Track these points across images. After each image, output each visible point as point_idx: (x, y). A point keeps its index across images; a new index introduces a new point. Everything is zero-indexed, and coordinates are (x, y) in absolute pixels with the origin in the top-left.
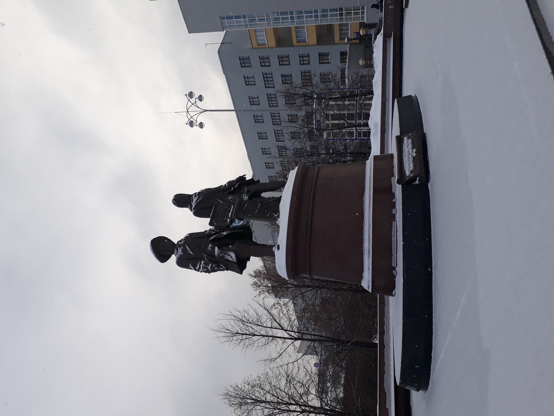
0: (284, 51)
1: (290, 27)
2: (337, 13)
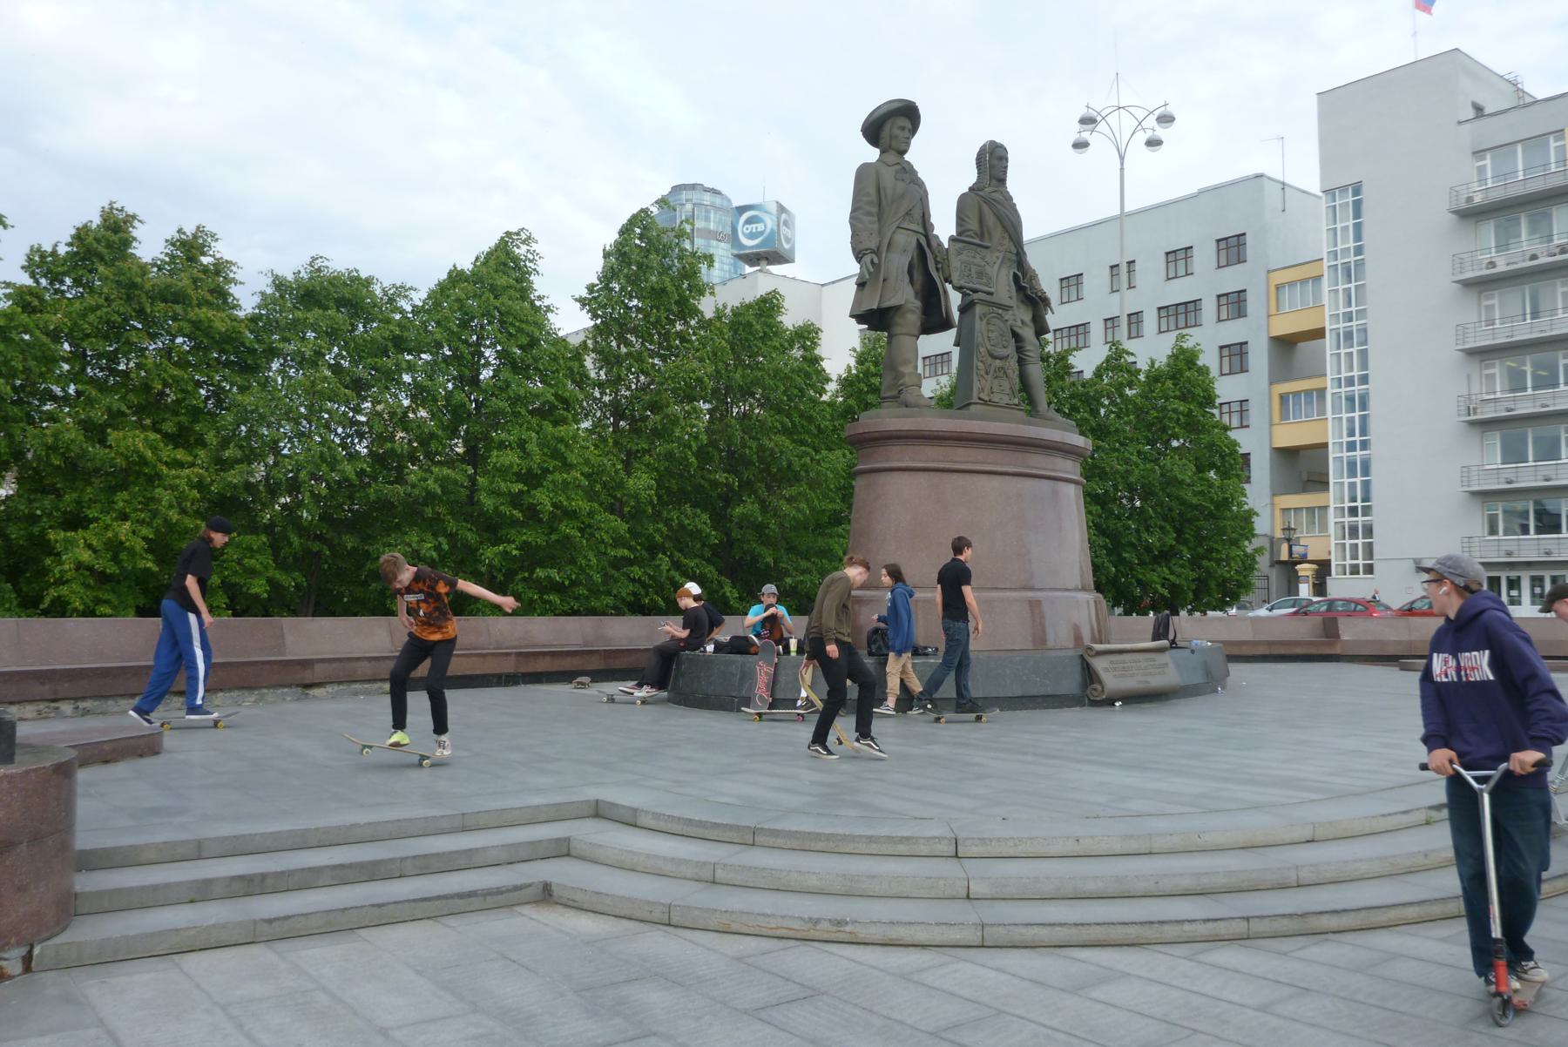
0: (1259, 357)
1: (1325, 375)
2: (1359, 499)
